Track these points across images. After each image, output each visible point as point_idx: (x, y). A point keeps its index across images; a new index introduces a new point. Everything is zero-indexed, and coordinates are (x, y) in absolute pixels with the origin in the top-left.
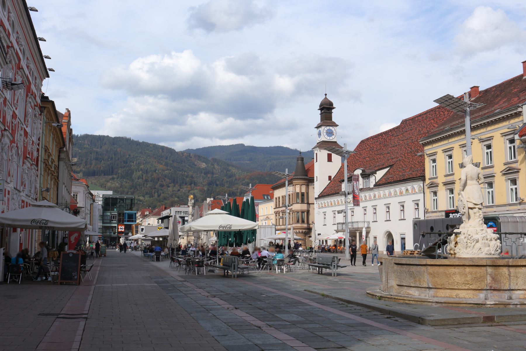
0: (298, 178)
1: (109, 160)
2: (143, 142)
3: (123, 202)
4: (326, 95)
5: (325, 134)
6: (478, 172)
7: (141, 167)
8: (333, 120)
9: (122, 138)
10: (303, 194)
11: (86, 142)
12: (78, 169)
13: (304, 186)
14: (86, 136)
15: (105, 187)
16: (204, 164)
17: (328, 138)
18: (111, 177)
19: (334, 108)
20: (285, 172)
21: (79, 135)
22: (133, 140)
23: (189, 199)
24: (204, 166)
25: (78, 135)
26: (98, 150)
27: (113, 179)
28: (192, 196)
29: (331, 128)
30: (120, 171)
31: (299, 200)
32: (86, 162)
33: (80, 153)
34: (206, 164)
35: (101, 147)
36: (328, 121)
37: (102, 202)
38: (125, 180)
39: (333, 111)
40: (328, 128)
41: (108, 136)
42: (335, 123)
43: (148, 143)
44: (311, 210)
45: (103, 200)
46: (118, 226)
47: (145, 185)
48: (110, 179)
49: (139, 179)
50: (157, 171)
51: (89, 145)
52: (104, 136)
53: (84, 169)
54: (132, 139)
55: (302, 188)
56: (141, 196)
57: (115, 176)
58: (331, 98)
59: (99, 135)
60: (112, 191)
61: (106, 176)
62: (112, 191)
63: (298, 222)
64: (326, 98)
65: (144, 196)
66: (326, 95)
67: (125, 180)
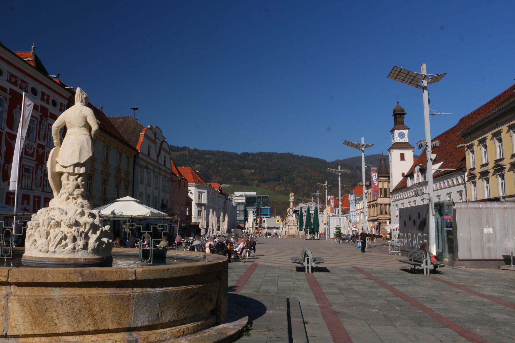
0: (383, 175)
1: (277, 170)
2: (302, 156)
3: (261, 200)
4: (398, 103)
5: (398, 136)
6: (82, 113)
7: (301, 174)
8: (405, 124)
9: (287, 153)
10: (385, 190)
11: (260, 158)
12: (255, 178)
13: (386, 182)
14: (260, 154)
15: (274, 190)
16: (349, 171)
17: (401, 140)
18: (278, 183)
19: (405, 114)
20: (338, 169)
21: (255, 153)
22: (170, 145)
23: (290, 196)
24: (349, 172)
25: (254, 153)
26: (269, 163)
27: (280, 184)
28: (293, 194)
29: (403, 131)
30: (285, 178)
31: (383, 195)
32: (260, 172)
33: (256, 166)
34: (351, 171)
35: (271, 161)
36: (401, 125)
37: (244, 200)
38: (288, 185)
39: (405, 116)
40: (400, 131)
41: (276, 153)
42: (406, 126)
43: (306, 157)
44: (198, 200)
45: (245, 199)
46: (257, 219)
47: (304, 188)
48: (278, 185)
49: (299, 184)
50: (313, 178)
51: (262, 160)
52: (273, 153)
53: (259, 178)
54: (293, 154)
55: (384, 184)
56: (300, 196)
57: (281, 182)
58: (402, 105)
59: (270, 153)
60: (256, 192)
61: (275, 182)
62: (256, 192)
63: (382, 213)
64: (398, 105)
65: (303, 196)
66: (398, 103)
67: (288, 185)
